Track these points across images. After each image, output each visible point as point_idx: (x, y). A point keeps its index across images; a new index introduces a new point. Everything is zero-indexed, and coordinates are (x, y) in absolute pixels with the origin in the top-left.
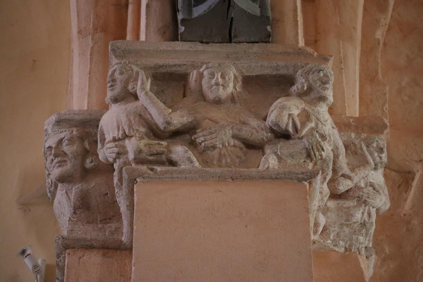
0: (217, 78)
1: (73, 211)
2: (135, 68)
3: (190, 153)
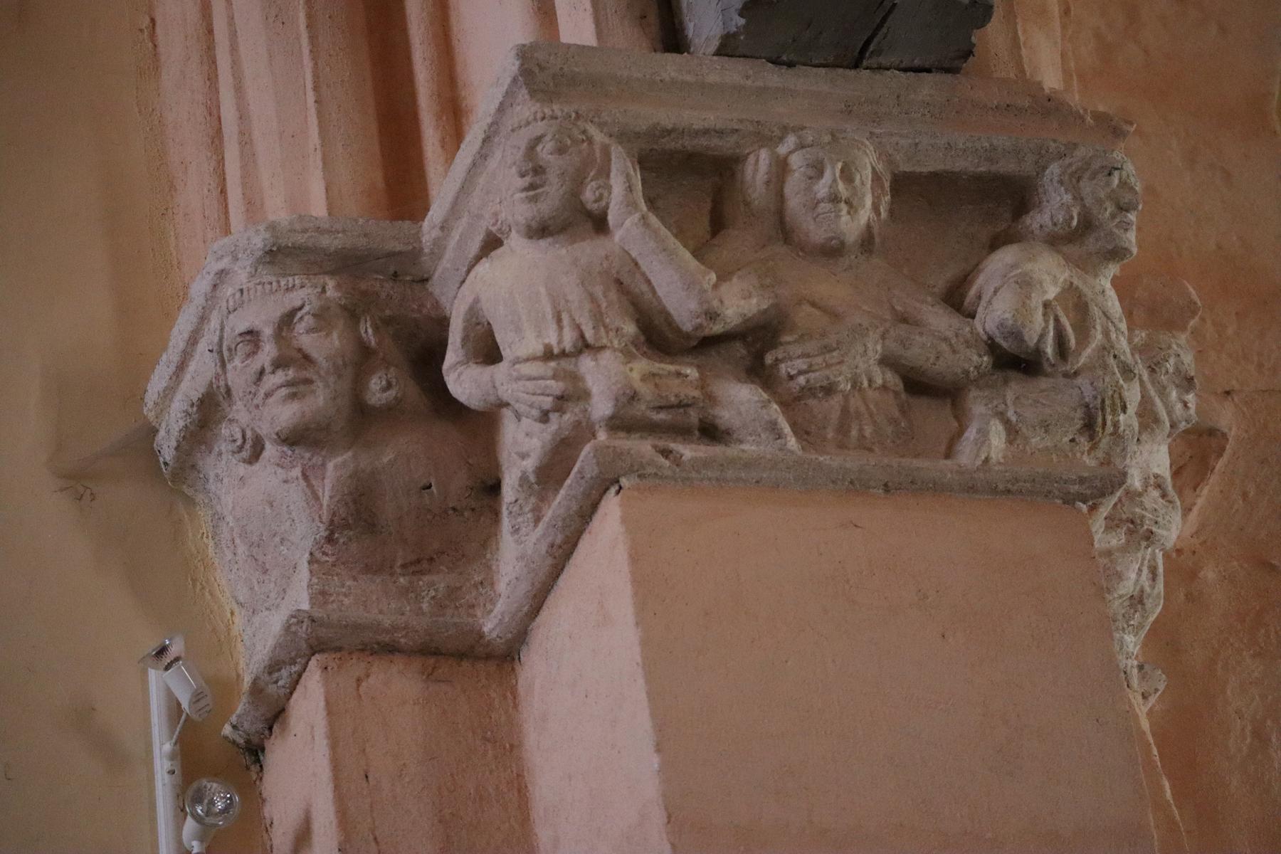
1: (325, 534)
2: (599, 137)
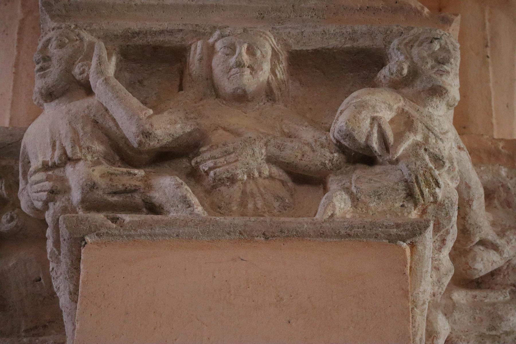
0: (240, 54)
2: (87, 37)
3: (187, 190)
